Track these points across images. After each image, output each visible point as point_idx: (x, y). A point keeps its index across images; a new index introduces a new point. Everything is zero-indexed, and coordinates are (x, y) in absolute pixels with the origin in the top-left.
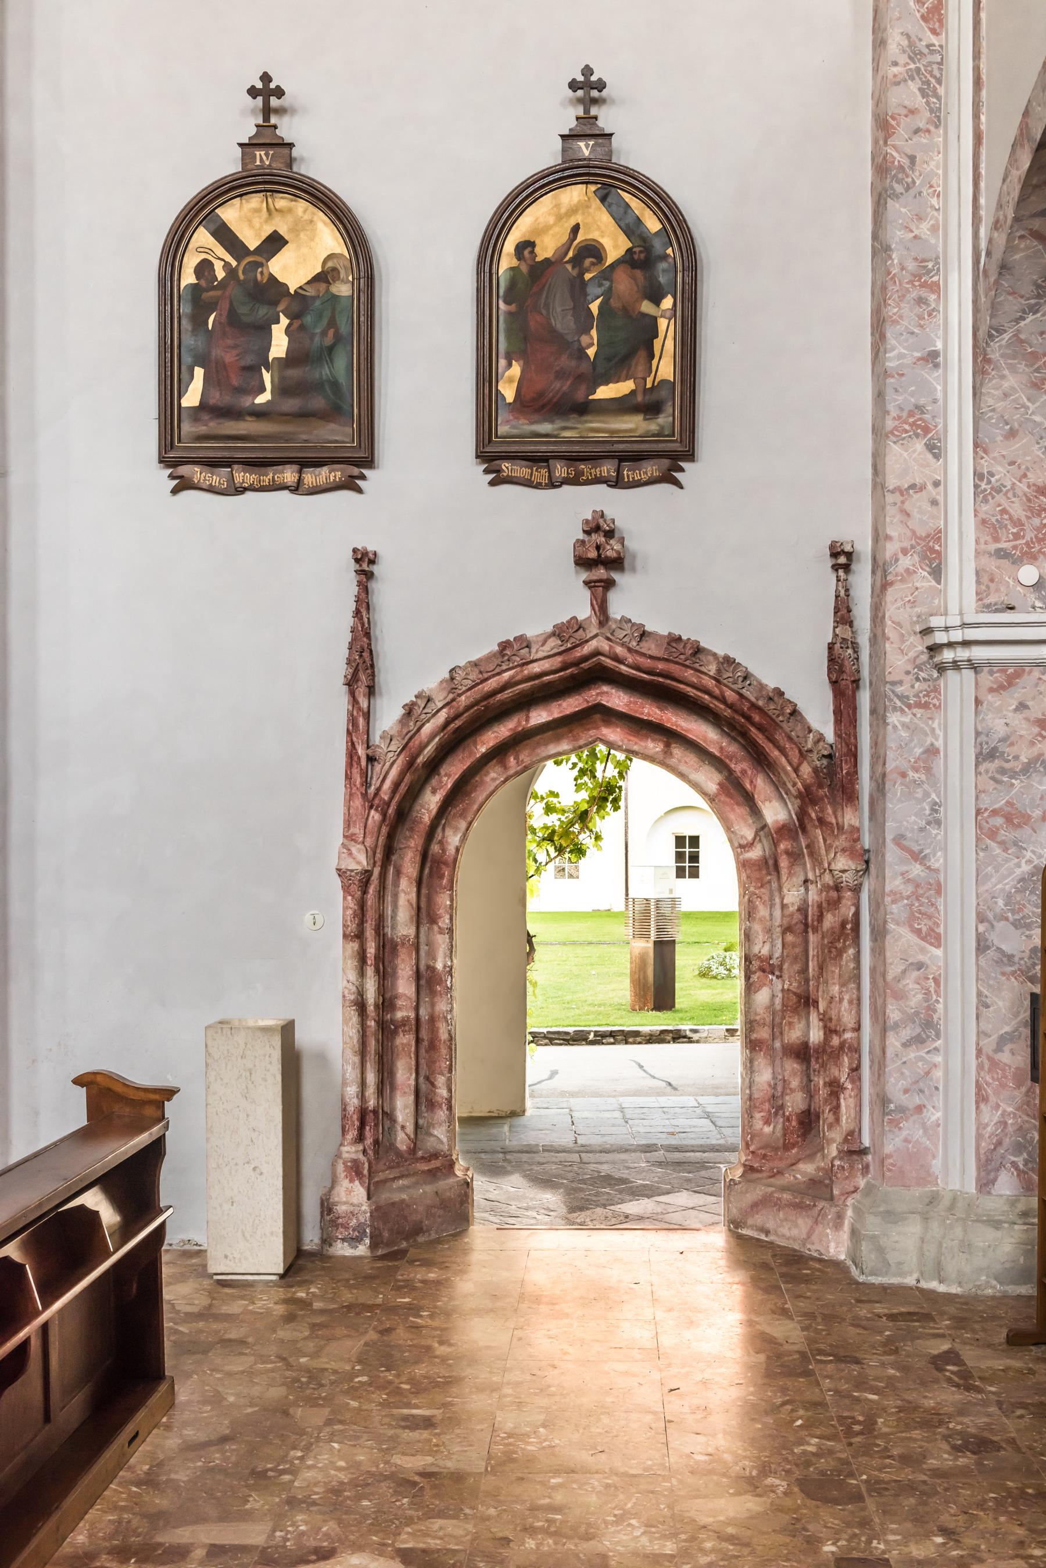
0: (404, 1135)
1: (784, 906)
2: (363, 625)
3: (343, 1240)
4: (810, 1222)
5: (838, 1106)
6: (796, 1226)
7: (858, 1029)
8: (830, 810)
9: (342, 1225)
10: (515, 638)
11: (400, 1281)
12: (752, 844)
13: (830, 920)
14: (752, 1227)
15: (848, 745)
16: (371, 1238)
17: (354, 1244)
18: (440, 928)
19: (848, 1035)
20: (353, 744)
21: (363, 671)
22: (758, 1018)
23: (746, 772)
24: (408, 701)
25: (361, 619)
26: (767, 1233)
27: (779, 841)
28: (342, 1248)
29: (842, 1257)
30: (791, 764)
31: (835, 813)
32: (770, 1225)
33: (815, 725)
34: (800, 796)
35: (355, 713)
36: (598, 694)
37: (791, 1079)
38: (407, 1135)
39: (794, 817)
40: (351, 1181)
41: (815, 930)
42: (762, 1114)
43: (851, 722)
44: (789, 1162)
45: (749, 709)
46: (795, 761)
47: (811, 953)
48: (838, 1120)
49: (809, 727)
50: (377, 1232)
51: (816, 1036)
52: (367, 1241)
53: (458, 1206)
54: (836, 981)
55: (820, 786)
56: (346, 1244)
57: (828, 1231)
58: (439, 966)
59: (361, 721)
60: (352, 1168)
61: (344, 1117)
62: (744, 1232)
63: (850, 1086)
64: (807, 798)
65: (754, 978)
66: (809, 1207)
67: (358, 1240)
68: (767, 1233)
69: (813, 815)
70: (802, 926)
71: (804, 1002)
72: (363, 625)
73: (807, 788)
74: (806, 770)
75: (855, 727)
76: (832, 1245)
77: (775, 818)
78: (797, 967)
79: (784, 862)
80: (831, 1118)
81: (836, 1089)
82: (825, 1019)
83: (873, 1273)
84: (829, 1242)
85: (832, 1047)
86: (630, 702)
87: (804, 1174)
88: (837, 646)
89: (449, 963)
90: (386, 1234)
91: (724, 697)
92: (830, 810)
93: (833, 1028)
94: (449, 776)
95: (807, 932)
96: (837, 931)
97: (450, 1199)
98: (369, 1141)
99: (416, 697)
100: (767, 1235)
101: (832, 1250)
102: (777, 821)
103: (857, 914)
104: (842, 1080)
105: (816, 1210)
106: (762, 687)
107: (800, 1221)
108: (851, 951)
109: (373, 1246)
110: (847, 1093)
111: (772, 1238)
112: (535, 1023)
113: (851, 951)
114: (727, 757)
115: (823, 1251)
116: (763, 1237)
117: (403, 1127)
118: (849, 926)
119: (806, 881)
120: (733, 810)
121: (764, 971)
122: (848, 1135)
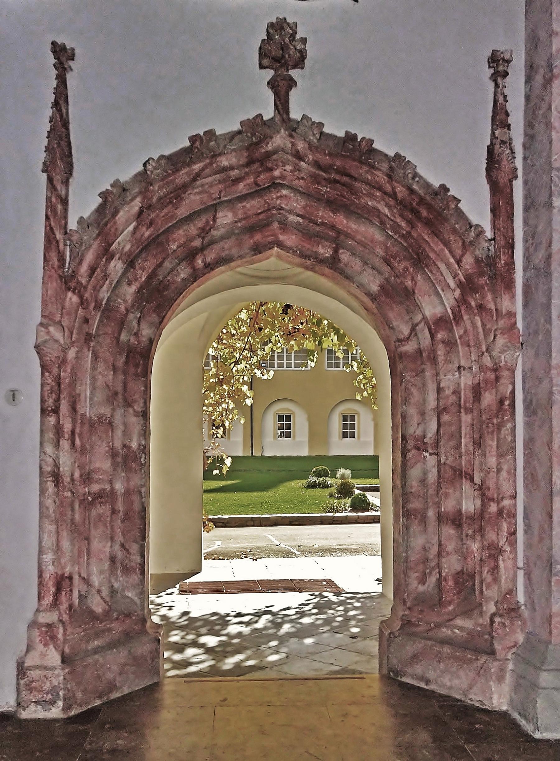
0: (99, 598)
1: (439, 390)
2: (61, 116)
3: (37, 703)
4: (471, 674)
5: (497, 567)
6: (458, 677)
7: (514, 497)
8: (489, 297)
9: (35, 688)
10: (205, 133)
11: (87, 752)
12: (408, 339)
13: (488, 398)
14: (413, 676)
15: (505, 238)
16: (65, 700)
17: (48, 707)
18: (134, 410)
19: (506, 503)
20: (51, 229)
21: (60, 157)
22: (413, 490)
23: (408, 269)
24: (104, 190)
25: (60, 110)
26: (428, 682)
27: (437, 332)
28: (35, 711)
29: (504, 708)
30: (453, 256)
31: (494, 300)
32: (431, 675)
33: (474, 219)
34: (460, 285)
35: (54, 200)
36: (278, 198)
37: (447, 543)
38: (102, 597)
39: (449, 311)
40: (46, 645)
41: (469, 411)
42: (417, 575)
43: (508, 217)
44: (446, 617)
45: (418, 204)
46: (458, 252)
47: (463, 432)
48: (496, 580)
49: (469, 224)
50: (70, 695)
51: (470, 505)
52: (60, 704)
53: (150, 661)
54: (494, 453)
55: (481, 274)
56: (39, 707)
57: (492, 683)
58: (134, 445)
59: (59, 207)
60: (46, 632)
61: (41, 584)
62: (404, 679)
63: (508, 549)
64: (468, 286)
65: (409, 455)
66: (470, 661)
67: (53, 703)
68: (428, 682)
69: (473, 303)
70: (457, 408)
71: (460, 474)
72: (61, 116)
73: (469, 278)
74: (468, 260)
75: (512, 221)
76: (495, 697)
77: (433, 311)
78: (452, 443)
79: (441, 351)
80: (489, 578)
81: (493, 552)
82: (482, 489)
83: (547, 729)
84: (492, 693)
85: (490, 514)
86: (307, 205)
87: (461, 628)
88: (497, 146)
89: (143, 442)
90: (79, 695)
91: (395, 193)
92: (489, 297)
93: (491, 496)
94: (143, 269)
95: (460, 412)
96: (494, 408)
97: (143, 656)
98: (64, 606)
99: (112, 186)
100: (427, 685)
101: (495, 701)
102: (435, 314)
103: (513, 392)
104: (501, 543)
105: (479, 663)
106: (428, 185)
107: (462, 673)
108: (509, 425)
109: (66, 708)
110: (506, 555)
111: (432, 687)
112: (250, 455)
113: (509, 425)
114: (391, 256)
115: (486, 702)
116: (422, 685)
117: (99, 591)
118: (507, 403)
119: (459, 368)
120: (392, 308)
121: (418, 449)
122: (507, 593)
